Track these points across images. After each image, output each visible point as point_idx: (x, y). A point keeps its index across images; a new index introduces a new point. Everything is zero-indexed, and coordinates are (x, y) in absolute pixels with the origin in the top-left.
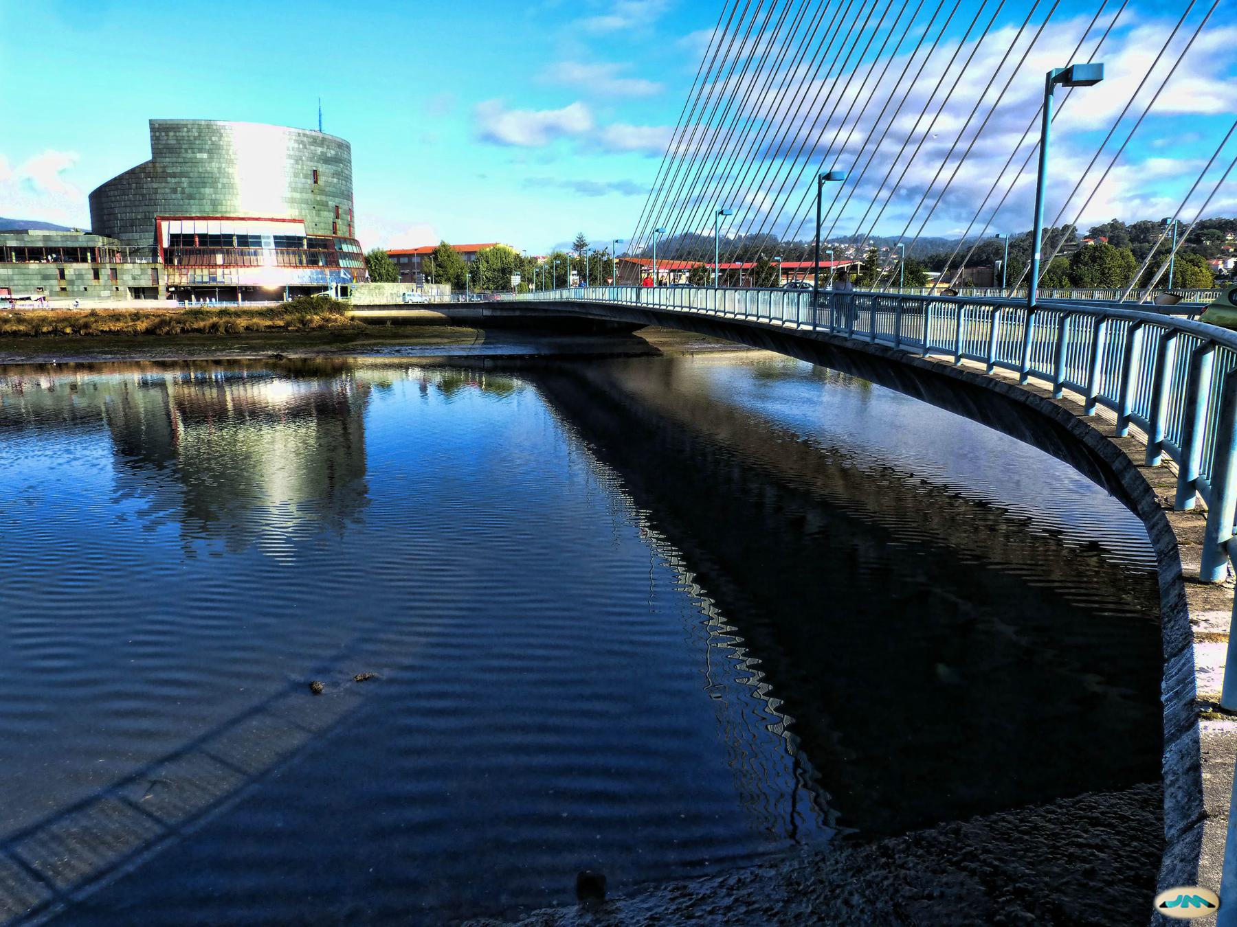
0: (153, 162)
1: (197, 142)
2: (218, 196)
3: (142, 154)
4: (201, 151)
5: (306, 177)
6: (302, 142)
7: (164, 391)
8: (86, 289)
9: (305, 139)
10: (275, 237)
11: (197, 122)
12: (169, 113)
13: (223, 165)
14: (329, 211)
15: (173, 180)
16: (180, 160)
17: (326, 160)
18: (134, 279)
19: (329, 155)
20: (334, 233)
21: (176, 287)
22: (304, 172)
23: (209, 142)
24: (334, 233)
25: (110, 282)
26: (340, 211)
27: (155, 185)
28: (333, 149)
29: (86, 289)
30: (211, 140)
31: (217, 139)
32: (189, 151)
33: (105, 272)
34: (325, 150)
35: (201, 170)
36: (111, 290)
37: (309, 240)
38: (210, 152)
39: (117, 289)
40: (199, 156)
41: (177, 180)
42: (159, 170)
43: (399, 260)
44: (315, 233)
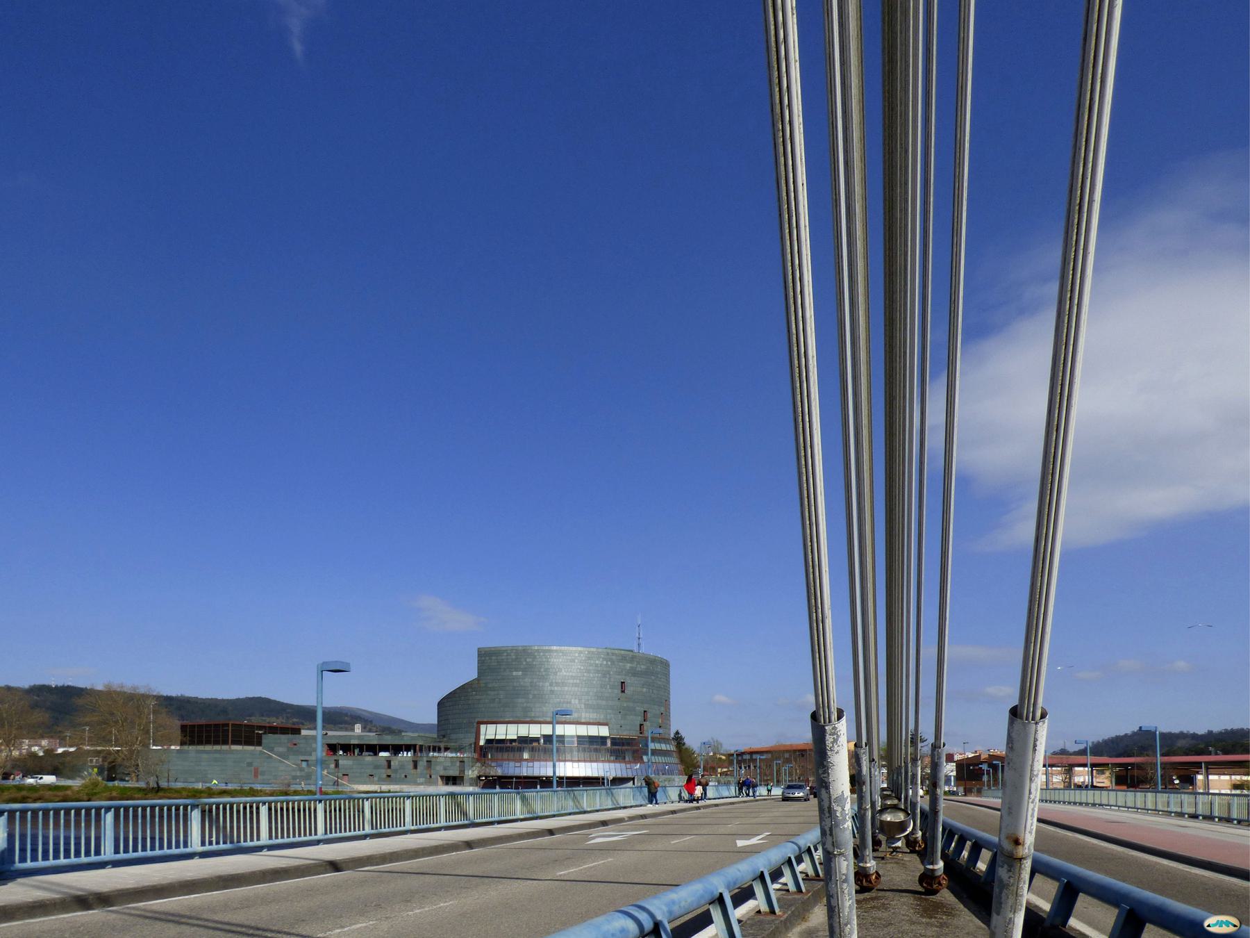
0: (478, 680)
1: (514, 663)
2: (528, 705)
3: (470, 674)
4: (516, 670)
5: (612, 687)
6: (611, 660)
7: (825, 847)
8: (406, 776)
9: (614, 657)
10: (677, 733)
11: (515, 648)
12: (496, 640)
13: (535, 680)
14: (635, 715)
15: (493, 693)
16: (499, 677)
17: (634, 673)
18: (445, 769)
19: (638, 669)
20: (641, 733)
21: (486, 777)
22: (611, 683)
23: (524, 663)
24: (641, 733)
25: (425, 772)
26: (649, 715)
27: (478, 697)
28: (643, 664)
29: (406, 776)
30: (526, 661)
31: (531, 660)
32: (508, 670)
33: (422, 764)
34: (634, 665)
35: (515, 684)
36: (426, 778)
37: (613, 739)
38: (524, 670)
39: (431, 776)
40: (514, 673)
41: (496, 692)
42: (483, 685)
43: (751, 757)
44: (620, 733)
